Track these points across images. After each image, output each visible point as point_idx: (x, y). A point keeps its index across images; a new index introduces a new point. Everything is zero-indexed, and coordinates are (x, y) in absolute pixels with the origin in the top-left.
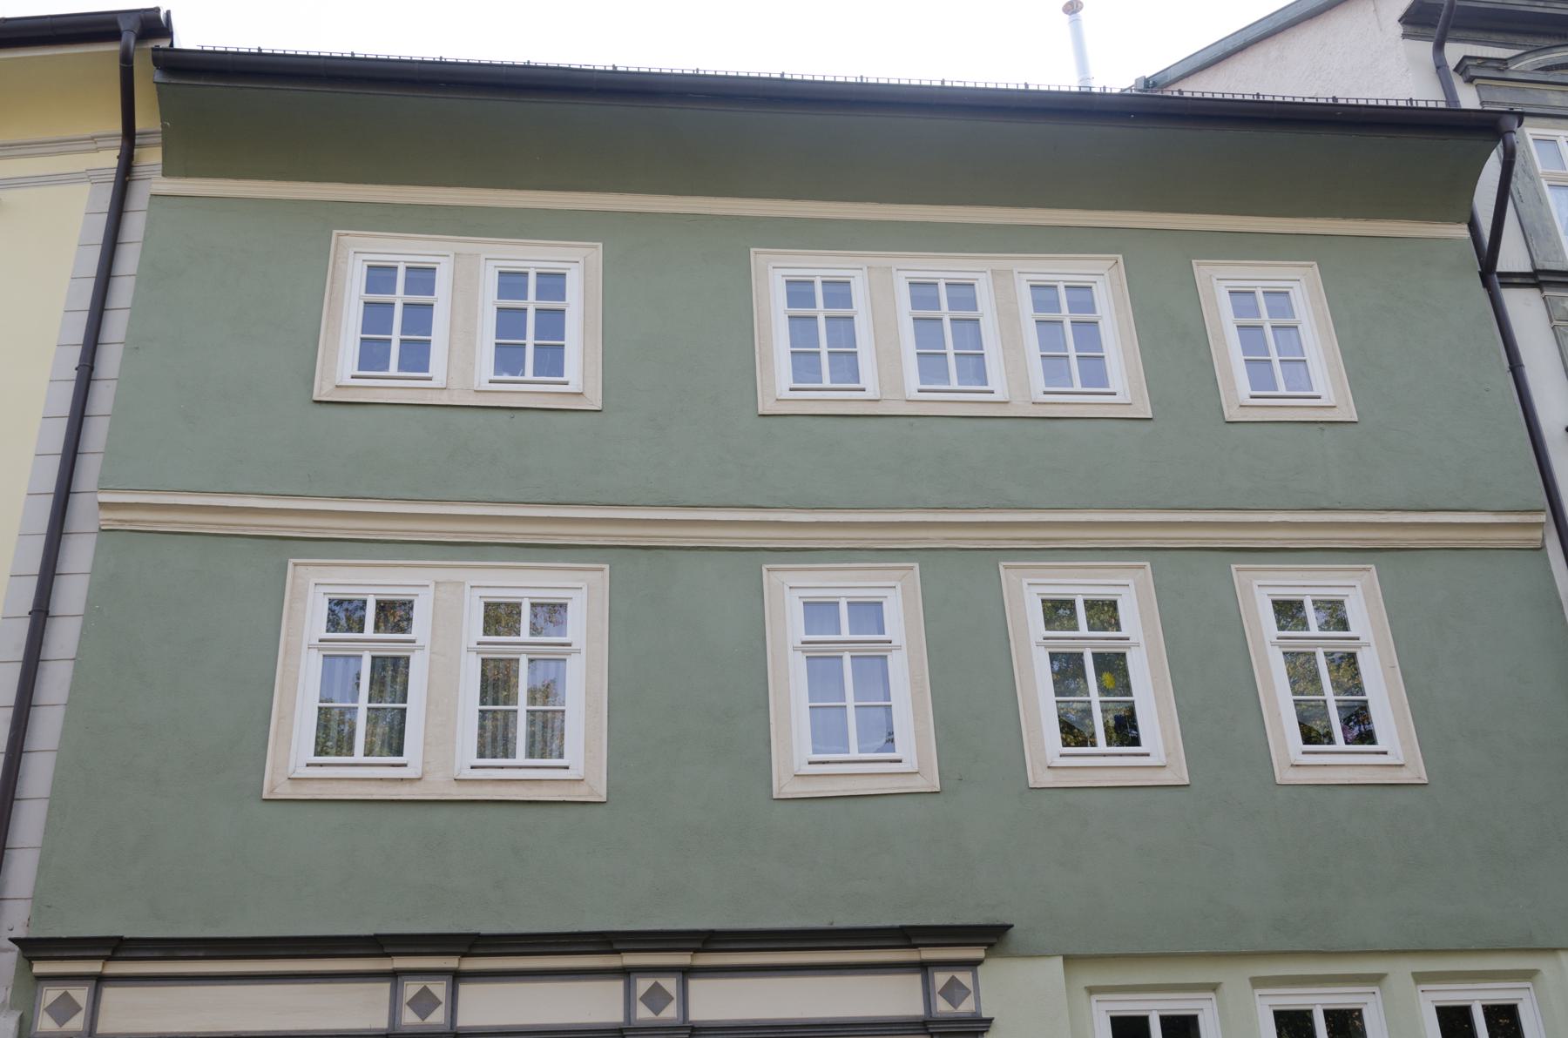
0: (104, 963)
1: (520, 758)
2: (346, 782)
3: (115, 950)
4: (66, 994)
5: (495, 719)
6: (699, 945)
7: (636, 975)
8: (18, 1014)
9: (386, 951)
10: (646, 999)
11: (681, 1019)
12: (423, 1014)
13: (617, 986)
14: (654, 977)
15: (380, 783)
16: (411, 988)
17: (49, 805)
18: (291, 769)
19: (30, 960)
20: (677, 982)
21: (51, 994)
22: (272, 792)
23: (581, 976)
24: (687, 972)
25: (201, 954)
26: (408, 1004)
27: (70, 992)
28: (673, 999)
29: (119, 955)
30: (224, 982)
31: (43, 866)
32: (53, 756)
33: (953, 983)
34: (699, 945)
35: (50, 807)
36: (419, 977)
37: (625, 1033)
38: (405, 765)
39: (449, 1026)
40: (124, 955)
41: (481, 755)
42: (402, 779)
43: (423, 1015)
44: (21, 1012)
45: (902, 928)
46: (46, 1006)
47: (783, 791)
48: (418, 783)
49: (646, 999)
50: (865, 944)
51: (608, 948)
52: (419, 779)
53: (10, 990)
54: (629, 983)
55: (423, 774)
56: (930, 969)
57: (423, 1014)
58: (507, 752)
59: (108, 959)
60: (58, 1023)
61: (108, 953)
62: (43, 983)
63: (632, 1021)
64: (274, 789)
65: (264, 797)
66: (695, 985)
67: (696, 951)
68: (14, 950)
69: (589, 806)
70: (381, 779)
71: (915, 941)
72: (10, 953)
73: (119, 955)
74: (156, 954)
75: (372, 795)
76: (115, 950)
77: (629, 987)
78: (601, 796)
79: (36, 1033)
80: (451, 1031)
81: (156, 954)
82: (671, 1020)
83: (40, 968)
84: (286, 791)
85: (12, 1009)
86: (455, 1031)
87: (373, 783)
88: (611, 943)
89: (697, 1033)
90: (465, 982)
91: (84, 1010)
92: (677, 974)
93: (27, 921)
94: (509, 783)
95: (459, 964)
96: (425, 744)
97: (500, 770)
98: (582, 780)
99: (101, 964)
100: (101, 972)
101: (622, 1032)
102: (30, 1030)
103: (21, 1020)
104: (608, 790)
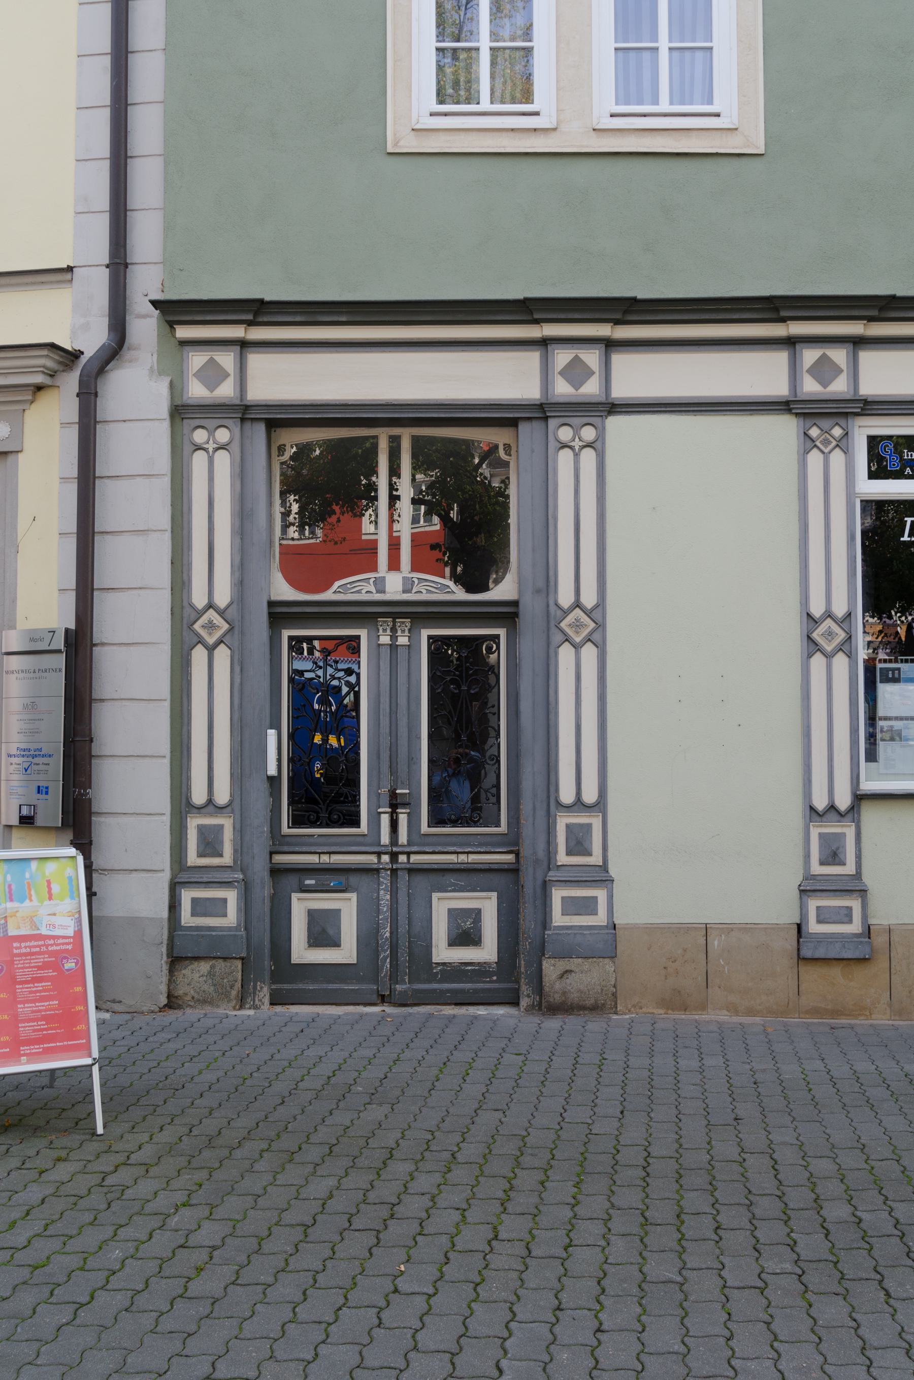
0: (246, 329)
1: (485, 104)
2: (474, 133)
3: (256, 314)
4: (212, 360)
5: (455, 58)
6: (874, 313)
7: (802, 345)
8: (168, 380)
9: (536, 316)
10: (565, 373)
11: (852, 392)
12: (577, 384)
13: (781, 357)
14: (822, 348)
15: (511, 134)
16: (562, 357)
17: (165, 162)
18: (414, 120)
19: (171, 325)
20: (847, 353)
21: (197, 359)
22: (396, 144)
23: (742, 347)
24: (610, 345)
25: (344, 319)
26: (560, 373)
27: (581, 356)
28: (842, 371)
29: (260, 319)
30: (368, 349)
31: (168, 228)
32: (159, 108)
33: (824, 360)
34: (874, 313)
35: (166, 164)
36: (570, 346)
37: (791, 406)
38: (537, 114)
39: (239, 399)
40: (265, 319)
41: (441, 102)
42: (535, 130)
43: (577, 385)
44: (170, 379)
45: (526, 300)
46: (194, 372)
47: (401, 143)
48: (553, 134)
49: (565, 373)
50: (577, 316)
51: (774, 316)
52: (555, 129)
53: (155, 356)
54: (795, 354)
55: (557, 124)
56: (798, 346)
57: (577, 384)
58: (471, 97)
59: (250, 323)
60: (208, 389)
61: (250, 317)
62: (187, 348)
63: (799, 394)
64: (398, 142)
65: (389, 151)
66: (619, 360)
67: (871, 319)
68: (153, 317)
69: (744, 160)
70: (512, 130)
71: (784, 313)
72: (148, 319)
73: (260, 319)
74: (298, 319)
75: (534, 147)
76: (256, 314)
77: (795, 357)
78: (757, 148)
79: (189, 398)
80: (606, 402)
81: (298, 319)
82: (841, 393)
83: (183, 332)
84: (411, 144)
85: (160, 375)
86: (610, 401)
87: (504, 134)
88: (777, 310)
89: (869, 407)
90: (617, 351)
91: (597, 373)
92: (847, 345)
93: (161, 286)
94: (654, 133)
95: (612, 332)
96: (558, 89)
97: (643, 118)
98: (736, 129)
99: (243, 329)
100: (244, 338)
101: (789, 406)
102: (182, 396)
103: (172, 385)
104: (765, 141)
